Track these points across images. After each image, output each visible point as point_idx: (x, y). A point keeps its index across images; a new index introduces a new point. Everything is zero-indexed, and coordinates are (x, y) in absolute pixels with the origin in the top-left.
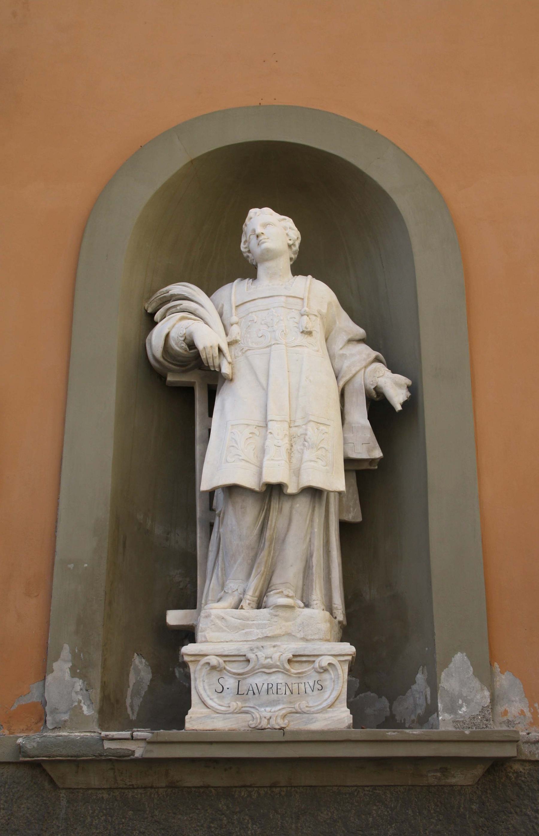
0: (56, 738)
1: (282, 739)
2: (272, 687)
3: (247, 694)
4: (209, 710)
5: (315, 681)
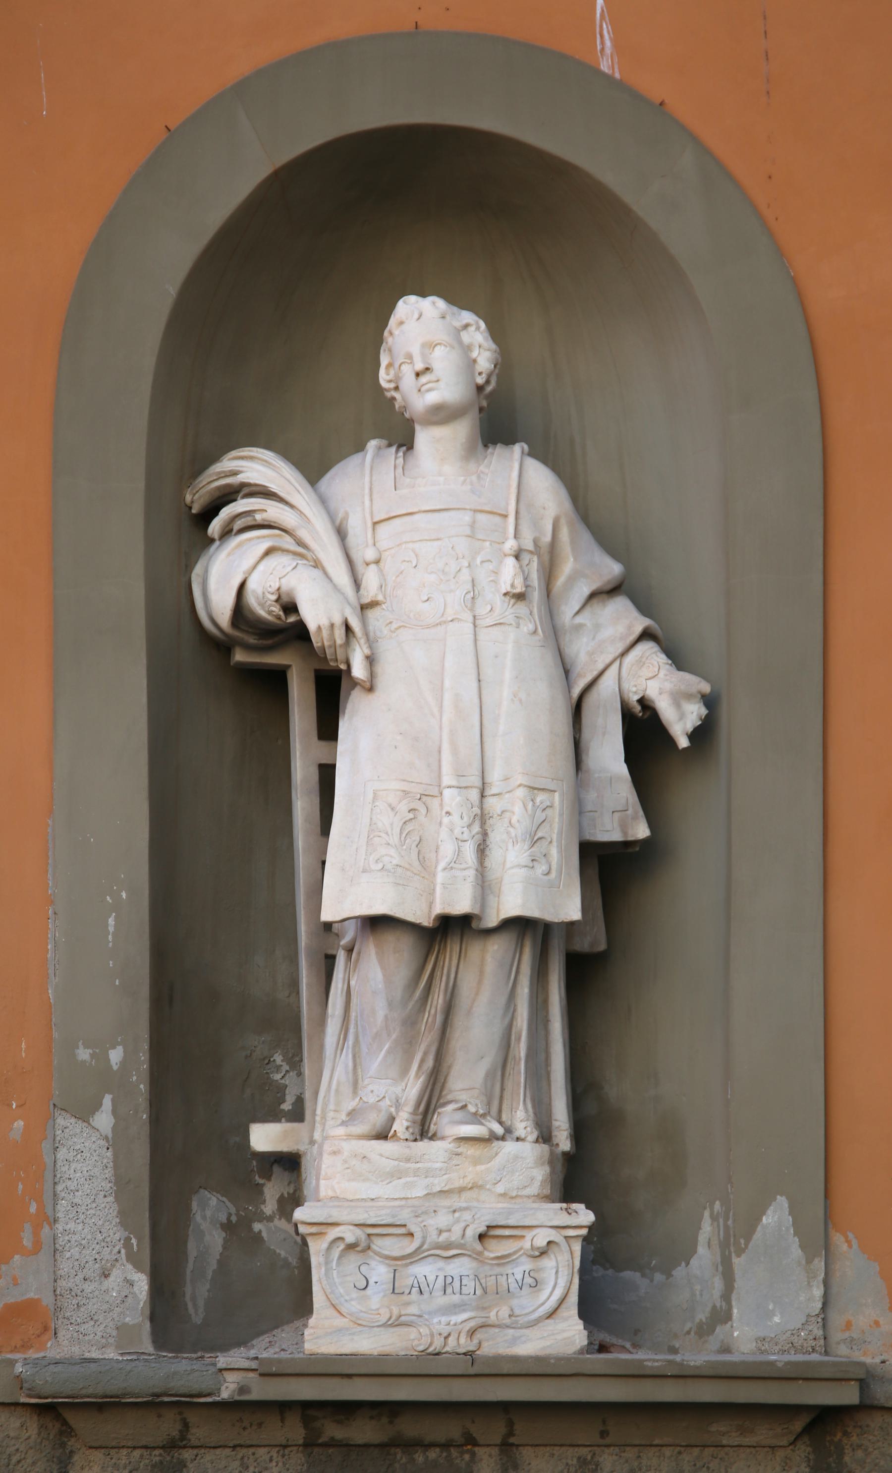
0: (83, 1366)
1: (472, 1371)
2: (452, 1282)
3: (410, 1293)
4: (345, 1320)
5: (524, 1271)
